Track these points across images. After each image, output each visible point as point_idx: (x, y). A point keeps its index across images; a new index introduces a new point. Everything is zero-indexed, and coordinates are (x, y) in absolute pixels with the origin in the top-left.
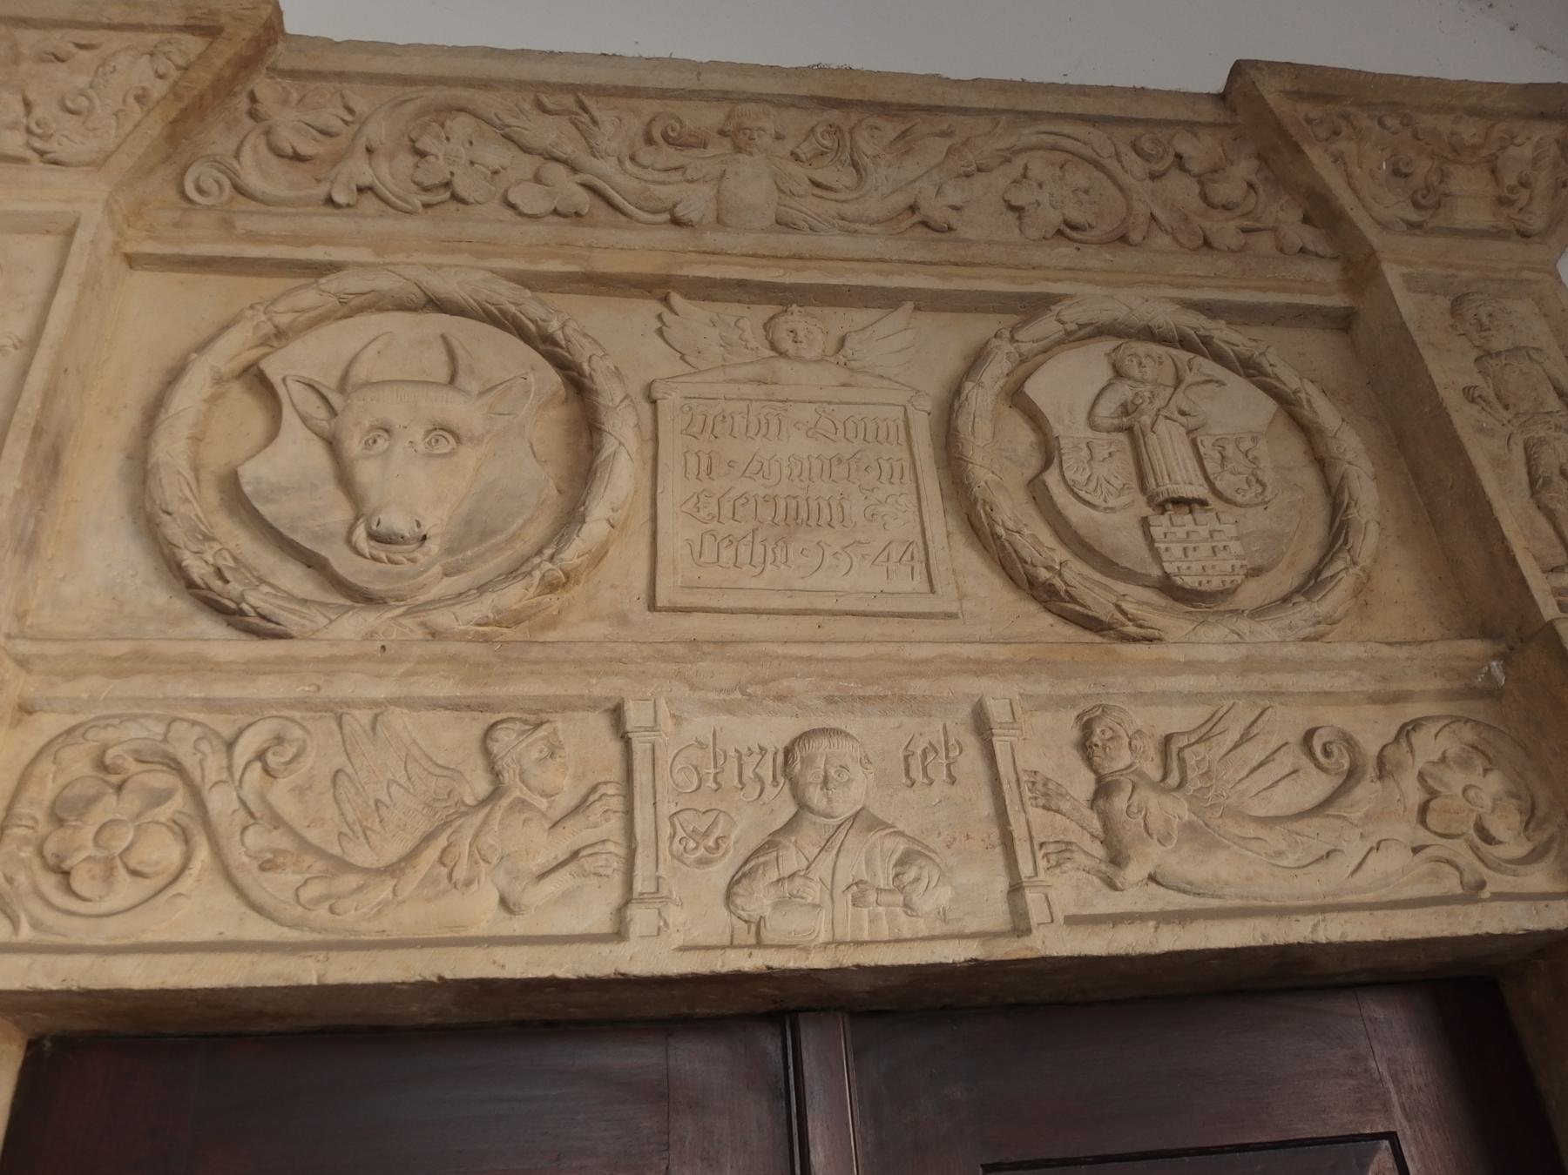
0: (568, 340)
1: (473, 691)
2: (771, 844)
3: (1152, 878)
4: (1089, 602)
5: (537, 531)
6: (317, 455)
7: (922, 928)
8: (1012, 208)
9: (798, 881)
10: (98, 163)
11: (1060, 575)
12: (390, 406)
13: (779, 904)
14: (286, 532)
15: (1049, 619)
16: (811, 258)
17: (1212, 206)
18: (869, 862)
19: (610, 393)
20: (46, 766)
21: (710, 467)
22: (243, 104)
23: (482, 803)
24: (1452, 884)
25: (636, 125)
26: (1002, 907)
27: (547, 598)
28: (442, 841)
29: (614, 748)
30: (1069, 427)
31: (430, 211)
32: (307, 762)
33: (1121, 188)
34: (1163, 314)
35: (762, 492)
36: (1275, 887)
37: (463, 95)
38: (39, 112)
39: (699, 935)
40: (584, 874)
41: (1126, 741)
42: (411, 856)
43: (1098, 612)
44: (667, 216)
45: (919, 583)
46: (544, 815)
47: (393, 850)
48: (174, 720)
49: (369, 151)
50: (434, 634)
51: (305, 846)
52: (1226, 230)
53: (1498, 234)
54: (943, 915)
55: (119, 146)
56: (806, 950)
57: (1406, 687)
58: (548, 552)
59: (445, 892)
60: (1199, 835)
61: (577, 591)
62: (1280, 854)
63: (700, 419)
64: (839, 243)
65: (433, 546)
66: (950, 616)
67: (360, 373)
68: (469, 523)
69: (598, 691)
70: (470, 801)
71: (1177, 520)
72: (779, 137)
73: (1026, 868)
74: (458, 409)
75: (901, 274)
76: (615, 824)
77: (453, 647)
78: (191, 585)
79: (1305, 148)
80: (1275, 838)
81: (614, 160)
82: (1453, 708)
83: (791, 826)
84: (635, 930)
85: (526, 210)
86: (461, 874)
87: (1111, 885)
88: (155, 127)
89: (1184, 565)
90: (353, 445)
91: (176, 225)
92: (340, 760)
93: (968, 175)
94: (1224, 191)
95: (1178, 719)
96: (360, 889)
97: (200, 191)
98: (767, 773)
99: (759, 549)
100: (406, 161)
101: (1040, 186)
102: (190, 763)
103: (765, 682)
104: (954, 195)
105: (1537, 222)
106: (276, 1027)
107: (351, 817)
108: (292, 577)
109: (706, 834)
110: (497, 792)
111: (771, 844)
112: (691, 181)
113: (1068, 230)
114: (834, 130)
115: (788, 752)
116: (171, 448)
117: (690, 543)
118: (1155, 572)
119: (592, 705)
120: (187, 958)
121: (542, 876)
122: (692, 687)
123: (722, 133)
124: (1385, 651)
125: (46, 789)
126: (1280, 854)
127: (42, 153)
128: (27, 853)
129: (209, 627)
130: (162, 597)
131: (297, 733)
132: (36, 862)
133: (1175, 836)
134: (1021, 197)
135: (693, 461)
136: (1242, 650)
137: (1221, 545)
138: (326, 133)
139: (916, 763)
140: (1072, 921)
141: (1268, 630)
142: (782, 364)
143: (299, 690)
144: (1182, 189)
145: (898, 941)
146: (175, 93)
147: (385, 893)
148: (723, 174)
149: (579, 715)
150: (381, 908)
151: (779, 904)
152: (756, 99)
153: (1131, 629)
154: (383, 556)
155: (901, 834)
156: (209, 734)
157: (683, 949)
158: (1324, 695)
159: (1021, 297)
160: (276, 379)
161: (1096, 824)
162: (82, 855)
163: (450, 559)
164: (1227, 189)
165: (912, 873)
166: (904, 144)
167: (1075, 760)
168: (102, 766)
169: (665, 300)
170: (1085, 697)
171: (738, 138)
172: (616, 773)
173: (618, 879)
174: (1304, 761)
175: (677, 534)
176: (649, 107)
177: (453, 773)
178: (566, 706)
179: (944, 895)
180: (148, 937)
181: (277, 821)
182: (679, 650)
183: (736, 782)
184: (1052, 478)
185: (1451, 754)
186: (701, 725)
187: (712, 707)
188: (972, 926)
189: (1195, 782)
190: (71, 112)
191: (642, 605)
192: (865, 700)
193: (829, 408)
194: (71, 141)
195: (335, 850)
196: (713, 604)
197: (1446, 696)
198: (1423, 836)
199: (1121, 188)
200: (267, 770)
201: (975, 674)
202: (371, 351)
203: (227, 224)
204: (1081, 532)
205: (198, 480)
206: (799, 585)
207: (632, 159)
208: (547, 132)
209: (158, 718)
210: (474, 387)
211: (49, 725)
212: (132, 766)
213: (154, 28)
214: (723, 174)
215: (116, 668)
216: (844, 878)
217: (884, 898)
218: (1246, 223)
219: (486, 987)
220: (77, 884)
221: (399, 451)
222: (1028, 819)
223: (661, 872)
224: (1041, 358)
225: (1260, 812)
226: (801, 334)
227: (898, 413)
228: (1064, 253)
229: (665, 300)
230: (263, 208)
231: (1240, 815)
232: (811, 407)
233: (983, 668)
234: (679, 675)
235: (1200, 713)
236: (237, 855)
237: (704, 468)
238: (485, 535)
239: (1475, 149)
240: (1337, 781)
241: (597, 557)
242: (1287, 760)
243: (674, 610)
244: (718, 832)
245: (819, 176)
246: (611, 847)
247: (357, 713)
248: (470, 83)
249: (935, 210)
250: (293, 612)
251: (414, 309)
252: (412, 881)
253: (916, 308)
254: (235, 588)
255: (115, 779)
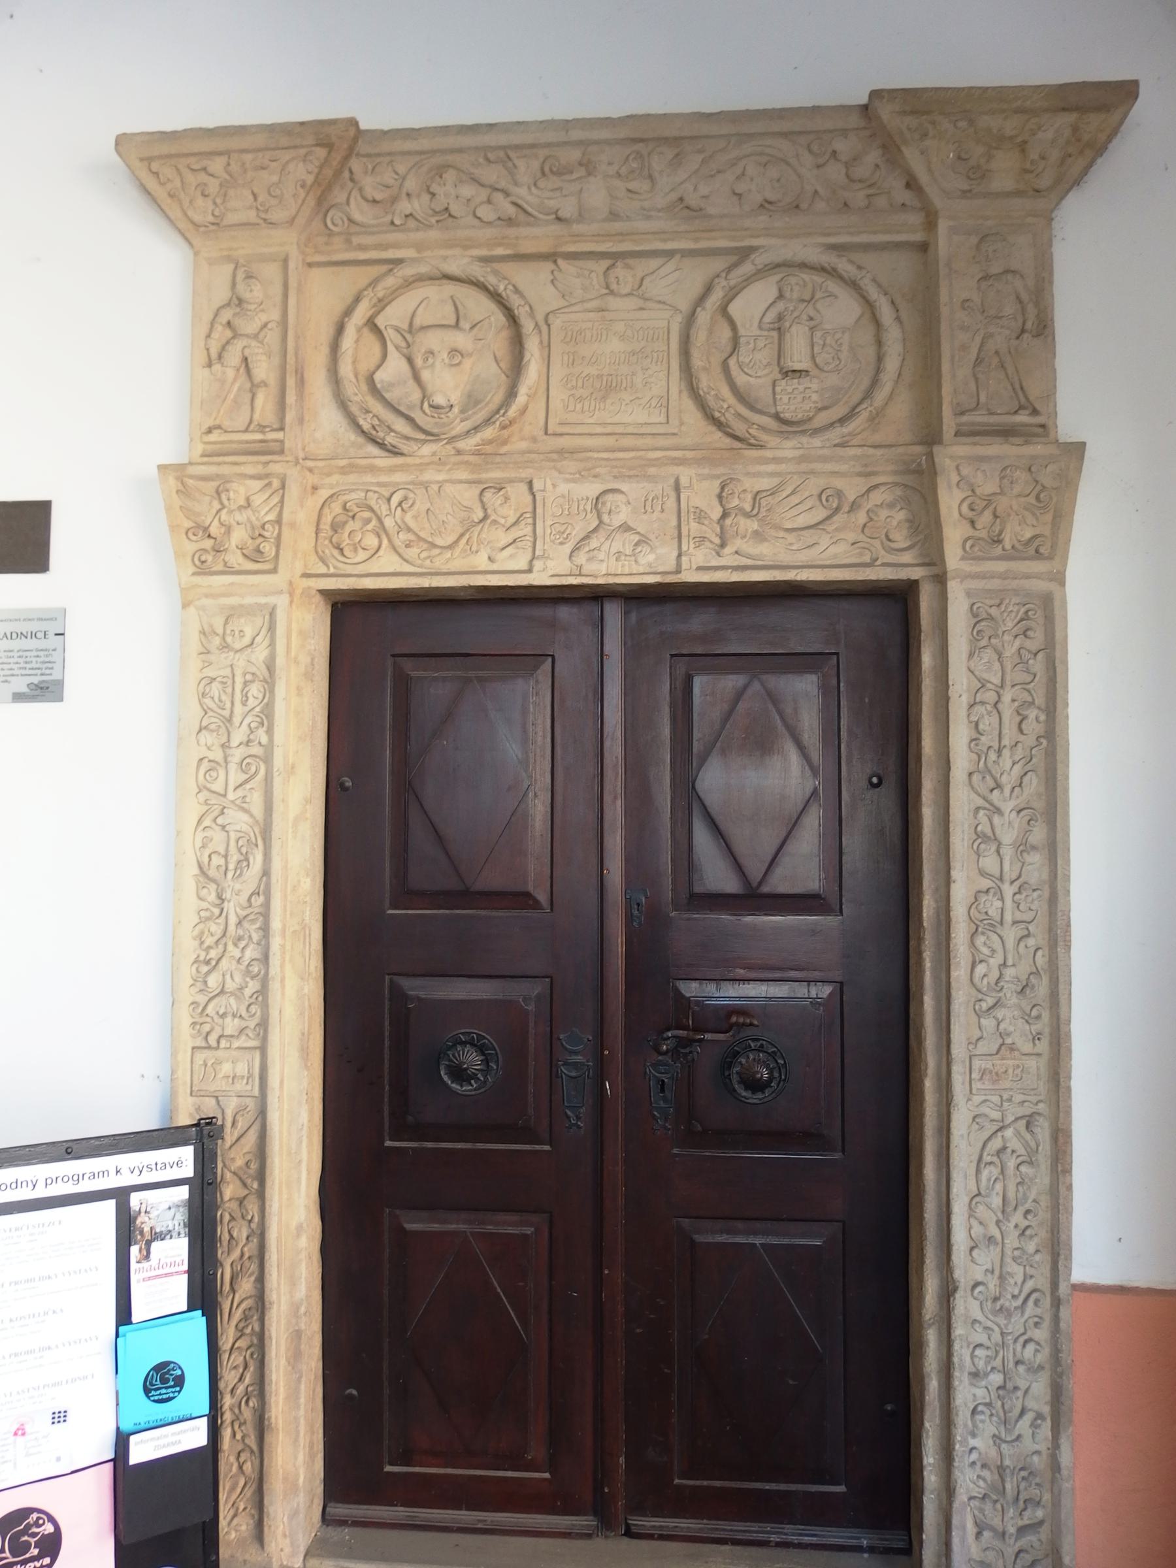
0: (507, 295)
1: (475, 477)
2: (587, 537)
3: (736, 552)
4: (735, 428)
5: (498, 398)
6: (404, 365)
7: (641, 570)
8: (735, 194)
9: (596, 552)
10: (292, 221)
11: (724, 415)
12: (432, 340)
13: (589, 560)
14: (396, 406)
15: (720, 434)
16: (628, 234)
17: (852, 181)
18: (624, 545)
19: (527, 326)
20: (326, 510)
21: (574, 360)
22: (346, 174)
23: (481, 521)
24: (867, 558)
25: (536, 164)
26: (674, 562)
27: (503, 432)
28: (467, 536)
29: (529, 498)
30: (748, 329)
31: (440, 224)
32: (416, 507)
33: (799, 176)
34: (813, 255)
35: (596, 373)
36: (785, 558)
37: (450, 158)
38: (260, 199)
39: (558, 571)
40: (518, 548)
41: (737, 495)
42: (456, 542)
43: (738, 434)
44: (554, 216)
45: (662, 419)
46: (503, 526)
47: (450, 540)
48: (368, 491)
49: (408, 195)
50: (459, 452)
51: (420, 539)
52: (858, 198)
53: (1018, 193)
54: (650, 565)
55: (298, 212)
56: (596, 577)
57: (875, 469)
58: (502, 412)
59: (469, 555)
60: (758, 536)
61: (515, 427)
62: (791, 544)
63: (570, 333)
64: (642, 225)
65: (456, 410)
66: (674, 434)
67: (418, 322)
68: (469, 396)
69: (523, 475)
70: (476, 520)
71: (790, 382)
72: (610, 164)
73: (684, 548)
74: (461, 340)
75: (673, 240)
76: (529, 529)
77: (466, 458)
78: (363, 432)
79: (903, 148)
80: (791, 538)
81: (525, 188)
82: (898, 479)
83: (595, 530)
84: (535, 569)
85: (485, 220)
86: (474, 548)
87: (718, 554)
88: (311, 202)
89: (787, 407)
90: (419, 362)
91: (327, 244)
92: (428, 505)
93: (712, 176)
94: (860, 171)
95: (765, 483)
96: (439, 554)
97: (333, 224)
98: (588, 508)
99: (593, 403)
100: (426, 198)
101: (752, 180)
102: (376, 508)
103: (589, 470)
104: (704, 190)
105: (1045, 182)
106: (415, 599)
107: (434, 527)
108: (401, 425)
109: (563, 533)
110: (486, 517)
111: (587, 537)
112: (565, 196)
113: (766, 205)
114: (639, 156)
115: (597, 499)
116: (346, 369)
117: (563, 400)
118: (773, 411)
119: (521, 480)
120: (386, 578)
121: (503, 549)
122: (560, 473)
123: (580, 164)
124: (871, 451)
125: (328, 519)
126: (791, 544)
127: (265, 220)
128: (327, 542)
129: (373, 450)
130: (353, 436)
131: (411, 495)
132: (330, 545)
133: (748, 536)
134: (741, 188)
135: (566, 358)
136: (801, 452)
137: (808, 396)
138: (388, 187)
139: (649, 503)
140: (699, 568)
141: (817, 442)
142: (610, 298)
143: (411, 478)
144: (835, 171)
145: (631, 574)
146: (316, 182)
147: (448, 555)
148: (581, 190)
149: (516, 484)
150: (448, 560)
151: (589, 560)
152: (597, 142)
153: (753, 441)
154: (436, 415)
155: (638, 533)
156: (381, 496)
157: (552, 576)
158: (834, 473)
159: (737, 248)
160: (382, 328)
161: (718, 530)
162: (345, 543)
163: (463, 416)
164: (862, 171)
165: (639, 549)
166: (677, 161)
167: (716, 502)
168: (344, 508)
169: (555, 262)
170: (724, 474)
171: (589, 167)
172: (530, 509)
173: (530, 549)
174: (818, 503)
175: (558, 395)
176: (542, 153)
177: (469, 509)
178: (511, 481)
179: (651, 557)
180: (372, 571)
181: (409, 530)
182: (555, 456)
183: (576, 512)
184: (732, 362)
185: (887, 501)
186: (563, 488)
187: (568, 481)
188: (661, 569)
189: (763, 513)
190: (274, 197)
191: (542, 433)
192: (630, 477)
193: (631, 323)
194: (278, 215)
195: (430, 540)
196: (571, 432)
197: (895, 473)
198: (861, 537)
199: (799, 176)
200: (403, 510)
201: (677, 465)
202: (420, 309)
203: (348, 241)
204: (741, 390)
205: (357, 380)
206: (609, 421)
207: (535, 185)
208: (491, 174)
209: (362, 490)
210: (467, 326)
211: (324, 493)
212: (356, 509)
213: (302, 146)
214: (581, 190)
215: (343, 471)
216: (613, 550)
217: (628, 558)
218: (871, 191)
219: (485, 588)
220: (345, 553)
221: (438, 364)
222: (692, 527)
223: (546, 547)
224: (745, 284)
225: (789, 525)
226: (621, 279)
227: (665, 323)
228: (763, 219)
229: (555, 262)
230: (363, 229)
231: (778, 527)
232: (623, 323)
233: (682, 462)
234: (555, 468)
235: (775, 481)
236: (397, 542)
237: (571, 361)
238: (477, 402)
239: (1011, 138)
240: (829, 512)
241: (523, 411)
242: (808, 504)
243: (555, 434)
244: (568, 532)
245: (633, 185)
246: (527, 538)
247: (432, 486)
248: (453, 151)
249: (693, 200)
250: (404, 444)
251: (438, 279)
252: (458, 551)
253: (682, 256)
254: (381, 434)
255: (351, 514)
